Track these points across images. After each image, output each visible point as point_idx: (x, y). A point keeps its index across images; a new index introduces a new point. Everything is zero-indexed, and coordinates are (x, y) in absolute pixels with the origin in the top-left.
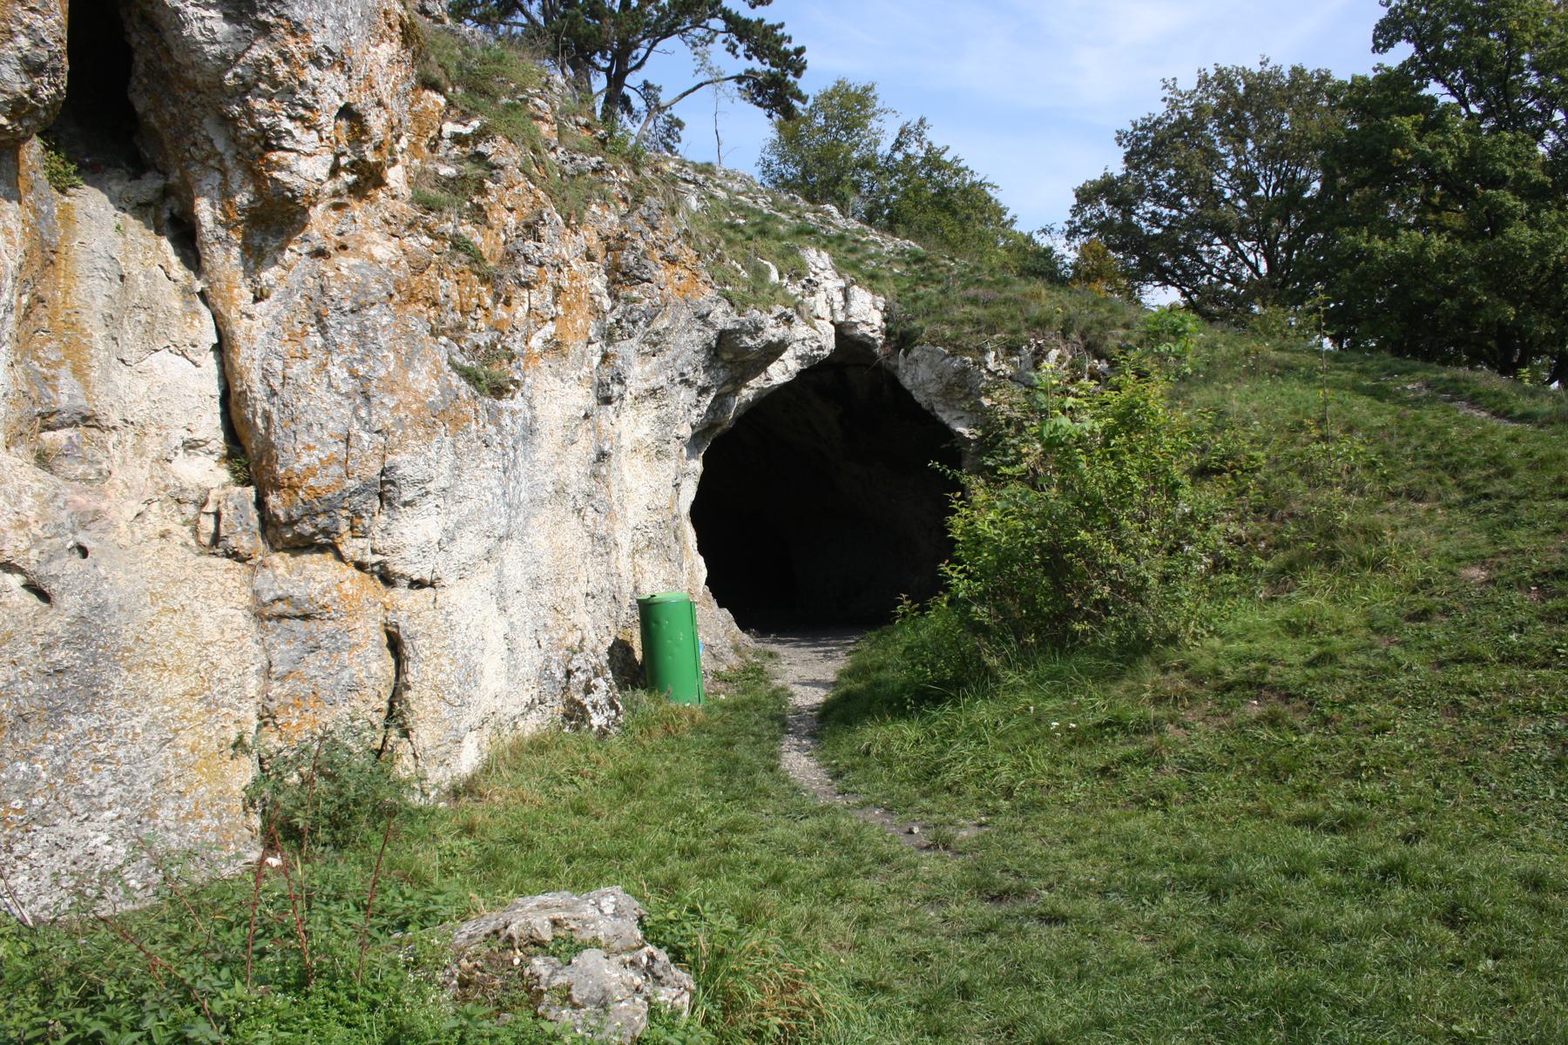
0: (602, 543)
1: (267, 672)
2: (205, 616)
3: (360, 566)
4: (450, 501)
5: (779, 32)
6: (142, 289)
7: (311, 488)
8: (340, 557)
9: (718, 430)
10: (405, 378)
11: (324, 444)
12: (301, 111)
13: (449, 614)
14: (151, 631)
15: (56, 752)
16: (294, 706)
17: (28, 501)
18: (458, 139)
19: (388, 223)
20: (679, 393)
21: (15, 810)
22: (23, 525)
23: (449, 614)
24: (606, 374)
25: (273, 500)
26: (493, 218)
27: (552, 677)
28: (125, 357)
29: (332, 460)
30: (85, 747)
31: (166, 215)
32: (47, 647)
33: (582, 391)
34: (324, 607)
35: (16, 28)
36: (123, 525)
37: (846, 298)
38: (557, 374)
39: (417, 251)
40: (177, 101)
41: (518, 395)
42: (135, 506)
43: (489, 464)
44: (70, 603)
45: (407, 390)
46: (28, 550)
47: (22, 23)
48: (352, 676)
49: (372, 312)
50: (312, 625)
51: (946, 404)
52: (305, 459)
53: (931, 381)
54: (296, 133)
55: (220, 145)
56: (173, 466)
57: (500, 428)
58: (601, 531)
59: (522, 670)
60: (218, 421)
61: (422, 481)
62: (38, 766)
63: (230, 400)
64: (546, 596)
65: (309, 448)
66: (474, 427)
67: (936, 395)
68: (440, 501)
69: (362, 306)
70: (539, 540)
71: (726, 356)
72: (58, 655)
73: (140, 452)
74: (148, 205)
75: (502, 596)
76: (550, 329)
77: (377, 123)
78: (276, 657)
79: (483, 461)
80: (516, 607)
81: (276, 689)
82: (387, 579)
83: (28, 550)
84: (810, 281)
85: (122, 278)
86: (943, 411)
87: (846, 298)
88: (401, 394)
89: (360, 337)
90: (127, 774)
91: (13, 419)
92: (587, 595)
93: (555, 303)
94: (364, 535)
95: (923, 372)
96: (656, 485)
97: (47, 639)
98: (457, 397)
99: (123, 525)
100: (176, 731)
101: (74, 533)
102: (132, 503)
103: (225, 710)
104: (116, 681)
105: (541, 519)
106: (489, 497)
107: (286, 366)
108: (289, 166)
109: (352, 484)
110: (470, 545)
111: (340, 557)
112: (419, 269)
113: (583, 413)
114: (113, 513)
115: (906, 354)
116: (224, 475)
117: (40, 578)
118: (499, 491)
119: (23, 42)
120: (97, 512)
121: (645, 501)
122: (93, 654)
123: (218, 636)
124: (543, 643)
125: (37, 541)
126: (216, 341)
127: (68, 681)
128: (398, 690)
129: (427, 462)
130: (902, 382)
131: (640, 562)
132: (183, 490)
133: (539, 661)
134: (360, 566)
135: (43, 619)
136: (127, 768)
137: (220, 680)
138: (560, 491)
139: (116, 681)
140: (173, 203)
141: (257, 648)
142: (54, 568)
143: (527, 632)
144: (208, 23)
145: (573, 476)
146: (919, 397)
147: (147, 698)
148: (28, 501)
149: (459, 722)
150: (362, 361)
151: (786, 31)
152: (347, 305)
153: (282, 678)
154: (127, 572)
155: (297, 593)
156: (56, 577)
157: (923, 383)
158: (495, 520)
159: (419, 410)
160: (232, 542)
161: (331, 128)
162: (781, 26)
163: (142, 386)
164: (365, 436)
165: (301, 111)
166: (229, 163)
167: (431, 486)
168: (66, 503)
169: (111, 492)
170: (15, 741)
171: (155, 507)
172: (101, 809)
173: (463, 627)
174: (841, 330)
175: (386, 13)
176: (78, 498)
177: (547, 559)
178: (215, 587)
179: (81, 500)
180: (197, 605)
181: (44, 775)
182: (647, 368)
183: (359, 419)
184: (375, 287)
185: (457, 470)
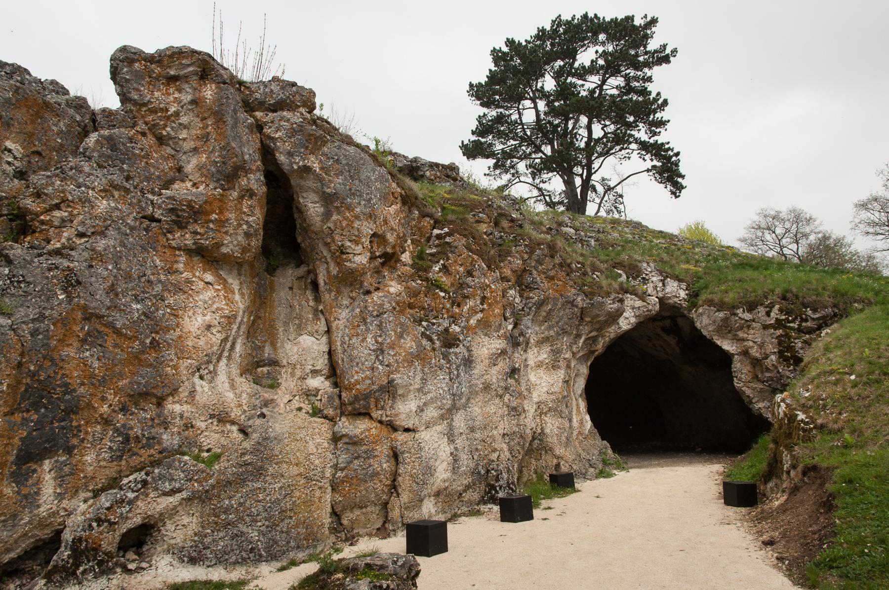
0: (516, 411)
1: (335, 467)
2: (311, 443)
3: (381, 422)
4: (421, 394)
5: (667, 146)
6: (297, 311)
7: (357, 389)
8: (371, 418)
9: (597, 353)
10: (399, 342)
11: (363, 371)
12: (354, 238)
13: (420, 443)
14: (287, 448)
15: (242, 497)
16: (346, 482)
17: (244, 396)
18: (438, 237)
19: (401, 277)
20: (563, 338)
21: (222, 520)
22: (240, 405)
23: (420, 443)
24: (516, 333)
25: (344, 394)
26: (452, 269)
27: (479, 473)
28: (290, 338)
29: (367, 377)
30: (253, 495)
31: (309, 281)
32: (243, 454)
33: (500, 341)
34: (361, 439)
35: (242, 222)
36: (282, 405)
37: (664, 285)
38: (486, 335)
39: (414, 287)
40: (310, 238)
41: (461, 346)
42: (288, 397)
43: (442, 377)
44: (255, 436)
45: (401, 347)
46: (240, 416)
47: (244, 220)
48: (374, 469)
49: (385, 316)
50: (357, 448)
51: (719, 336)
52: (356, 377)
53: (710, 324)
54: (353, 246)
55: (325, 253)
56: (307, 381)
57: (449, 362)
58: (514, 404)
59: (462, 469)
60: (326, 361)
61: (406, 386)
62: (233, 502)
63: (330, 353)
64: (478, 435)
65: (357, 372)
66: (433, 361)
67: (713, 331)
68: (417, 394)
69: (382, 314)
70: (476, 410)
71: (588, 319)
72: (247, 457)
73: (293, 375)
74: (302, 277)
75: (452, 435)
76: (480, 315)
77: (391, 238)
78: (340, 461)
79: (438, 376)
80: (460, 442)
81: (339, 474)
82: (395, 429)
83: (240, 416)
84: (643, 278)
85: (291, 306)
86: (718, 340)
87: (664, 285)
88: (397, 349)
89: (380, 326)
90: (269, 507)
91: (244, 364)
92: (504, 435)
93: (482, 304)
94: (383, 408)
95: (705, 320)
96: (552, 382)
97: (243, 451)
98: (425, 349)
99: (282, 405)
100: (292, 490)
101: (261, 408)
102: (287, 396)
103: (314, 482)
104: (270, 468)
105: (477, 400)
106: (441, 391)
107: (350, 339)
108: (350, 260)
109: (375, 387)
110: (431, 413)
111: (371, 418)
112: (415, 294)
113: (500, 351)
114: (279, 400)
115: (696, 311)
116: (327, 383)
117: (244, 427)
118: (446, 389)
119: (245, 227)
120: (272, 400)
121: (545, 389)
122: (262, 458)
123: (315, 450)
124: (475, 457)
125: (245, 411)
126: (326, 329)
127: (250, 468)
128: (395, 475)
129: (408, 377)
130: (696, 325)
131: (545, 418)
132: (309, 390)
133: (472, 465)
134: (381, 422)
135: (245, 443)
136: (269, 505)
137: (313, 469)
138: (487, 387)
139: (270, 468)
140: (312, 276)
141: (331, 456)
142: (250, 422)
143: (466, 452)
144: (316, 209)
145: (494, 380)
146: (705, 333)
147: (283, 476)
148: (244, 396)
149: (421, 492)
150: (380, 336)
151: (671, 146)
152: (375, 313)
153: (342, 470)
154: (280, 424)
155: (351, 433)
156: (251, 426)
157: (706, 326)
158: (445, 402)
159: (405, 356)
160: (325, 412)
161: (368, 242)
162: (668, 143)
163: (295, 349)
164: (380, 367)
165: (354, 238)
166: (329, 260)
167: (412, 388)
168: (260, 396)
169: (279, 392)
170: (225, 492)
171: (297, 398)
172: (257, 522)
173: (427, 449)
174: (661, 300)
175: (393, 193)
176: (265, 395)
177: (480, 418)
178: (317, 430)
179: (266, 395)
180: (308, 438)
181: (235, 506)
182: (543, 328)
183: (379, 360)
184: (387, 306)
185: (424, 381)
